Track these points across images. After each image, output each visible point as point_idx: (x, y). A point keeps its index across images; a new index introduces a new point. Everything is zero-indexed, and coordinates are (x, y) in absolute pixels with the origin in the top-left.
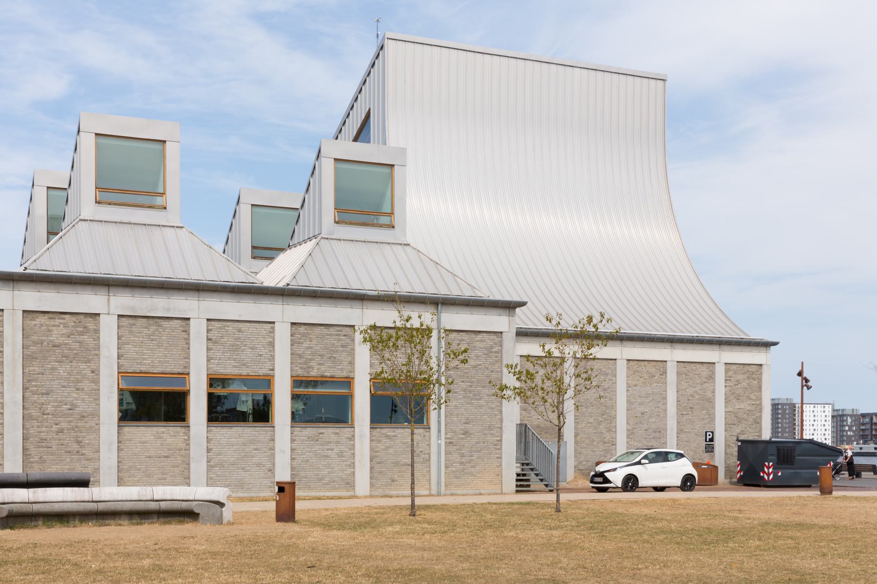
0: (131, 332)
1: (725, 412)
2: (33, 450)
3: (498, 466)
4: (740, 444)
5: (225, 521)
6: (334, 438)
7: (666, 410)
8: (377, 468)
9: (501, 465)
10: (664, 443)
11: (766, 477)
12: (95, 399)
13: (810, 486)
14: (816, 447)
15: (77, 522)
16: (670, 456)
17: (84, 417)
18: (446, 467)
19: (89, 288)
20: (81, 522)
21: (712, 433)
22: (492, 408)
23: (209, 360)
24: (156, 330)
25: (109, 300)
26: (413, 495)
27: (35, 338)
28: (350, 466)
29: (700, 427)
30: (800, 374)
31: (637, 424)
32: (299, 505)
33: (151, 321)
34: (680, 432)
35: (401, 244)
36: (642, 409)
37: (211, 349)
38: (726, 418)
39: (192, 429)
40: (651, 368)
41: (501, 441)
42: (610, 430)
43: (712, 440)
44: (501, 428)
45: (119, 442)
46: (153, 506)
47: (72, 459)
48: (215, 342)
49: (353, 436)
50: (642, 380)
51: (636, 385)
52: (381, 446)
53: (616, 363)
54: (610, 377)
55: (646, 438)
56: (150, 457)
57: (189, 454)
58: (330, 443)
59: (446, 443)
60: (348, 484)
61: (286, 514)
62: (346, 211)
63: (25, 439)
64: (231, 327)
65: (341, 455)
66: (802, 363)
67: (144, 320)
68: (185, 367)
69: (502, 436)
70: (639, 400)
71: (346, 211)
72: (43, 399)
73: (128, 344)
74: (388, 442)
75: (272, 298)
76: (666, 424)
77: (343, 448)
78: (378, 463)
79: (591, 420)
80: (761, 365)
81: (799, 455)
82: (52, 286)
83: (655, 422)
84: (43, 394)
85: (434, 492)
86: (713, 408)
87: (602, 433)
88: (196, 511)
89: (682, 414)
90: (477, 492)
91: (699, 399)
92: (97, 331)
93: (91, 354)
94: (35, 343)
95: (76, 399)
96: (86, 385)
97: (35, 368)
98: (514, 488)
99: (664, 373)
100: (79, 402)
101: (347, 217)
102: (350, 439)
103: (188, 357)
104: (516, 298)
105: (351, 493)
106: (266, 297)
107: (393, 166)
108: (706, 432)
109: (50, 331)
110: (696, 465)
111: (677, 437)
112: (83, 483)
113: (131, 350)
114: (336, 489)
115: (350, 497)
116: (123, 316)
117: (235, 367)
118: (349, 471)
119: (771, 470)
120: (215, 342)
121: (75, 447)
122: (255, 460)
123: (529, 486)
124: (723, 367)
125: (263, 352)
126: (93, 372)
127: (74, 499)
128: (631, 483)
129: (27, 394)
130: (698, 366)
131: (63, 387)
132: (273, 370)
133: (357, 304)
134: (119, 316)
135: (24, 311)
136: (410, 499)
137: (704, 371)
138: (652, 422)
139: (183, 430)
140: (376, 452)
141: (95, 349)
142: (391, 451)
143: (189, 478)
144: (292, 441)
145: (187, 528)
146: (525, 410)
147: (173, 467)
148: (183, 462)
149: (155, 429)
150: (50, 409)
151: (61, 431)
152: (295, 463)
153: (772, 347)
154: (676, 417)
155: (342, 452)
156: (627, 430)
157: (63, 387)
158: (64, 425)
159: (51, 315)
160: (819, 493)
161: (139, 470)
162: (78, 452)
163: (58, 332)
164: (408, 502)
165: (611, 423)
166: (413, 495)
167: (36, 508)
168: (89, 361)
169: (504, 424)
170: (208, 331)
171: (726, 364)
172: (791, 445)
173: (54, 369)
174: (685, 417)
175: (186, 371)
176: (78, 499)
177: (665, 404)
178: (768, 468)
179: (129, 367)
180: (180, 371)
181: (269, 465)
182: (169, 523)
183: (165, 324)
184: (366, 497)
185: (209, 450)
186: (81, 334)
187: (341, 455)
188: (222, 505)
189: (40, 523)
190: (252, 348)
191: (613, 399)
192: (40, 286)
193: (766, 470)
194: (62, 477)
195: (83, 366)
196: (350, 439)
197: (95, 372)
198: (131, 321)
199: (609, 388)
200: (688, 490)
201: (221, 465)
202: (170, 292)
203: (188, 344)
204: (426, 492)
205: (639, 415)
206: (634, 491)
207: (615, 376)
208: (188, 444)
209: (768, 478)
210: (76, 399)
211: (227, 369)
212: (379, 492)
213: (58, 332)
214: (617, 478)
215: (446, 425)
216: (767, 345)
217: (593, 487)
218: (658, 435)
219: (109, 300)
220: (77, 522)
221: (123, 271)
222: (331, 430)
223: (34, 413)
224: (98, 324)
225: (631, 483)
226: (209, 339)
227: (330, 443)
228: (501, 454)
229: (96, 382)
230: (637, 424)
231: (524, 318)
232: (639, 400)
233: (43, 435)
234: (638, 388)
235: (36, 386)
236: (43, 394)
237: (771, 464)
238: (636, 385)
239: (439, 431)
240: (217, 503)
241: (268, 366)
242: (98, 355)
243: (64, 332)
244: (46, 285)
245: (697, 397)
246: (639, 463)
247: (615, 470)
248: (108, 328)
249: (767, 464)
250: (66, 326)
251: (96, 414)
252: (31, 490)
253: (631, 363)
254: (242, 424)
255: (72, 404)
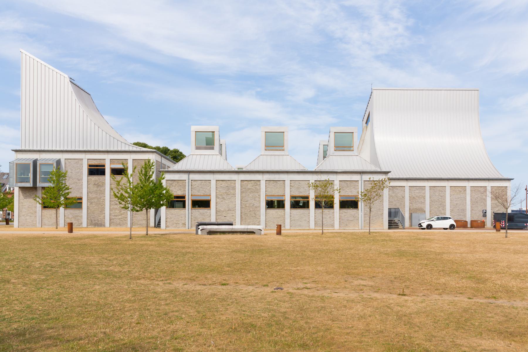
0: (269, 185)
1: (491, 203)
2: (243, 216)
3: (382, 221)
4: (494, 214)
5: (262, 234)
6: (328, 213)
7: (466, 203)
8: (342, 221)
9: (383, 221)
10: (465, 214)
11: (502, 226)
12: (259, 203)
13: (522, 229)
14: (524, 215)
15: (227, 234)
16: (448, 218)
17: (256, 207)
18: (364, 221)
19: (258, 173)
20: (228, 234)
21: (486, 210)
22: (380, 204)
23: (291, 191)
24: (276, 184)
25: (263, 176)
26: (370, 230)
27: (244, 187)
28: (333, 221)
29: (481, 208)
30: (526, 189)
31: (454, 207)
32: (282, 231)
33: (275, 182)
34: (472, 210)
35: (355, 155)
36: (456, 202)
37: (291, 189)
38: (491, 205)
39: (310, 210)
40: (460, 189)
41: (383, 213)
42: (443, 210)
43: (485, 213)
44: (383, 210)
45: (266, 214)
46: (246, 230)
47: (253, 218)
48: (293, 187)
49: (334, 212)
50: (457, 193)
51: (454, 195)
52: (343, 215)
53: (446, 188)
54: (443, 192)
55: (458, 212)
56: (274, 218)
57: (285, 218)
58: (326, 214)
59: (364, 214)
60: (332, 226)
61: (279, 233)
62: (338, 147)
63: (241, 213)
64: (297, 182)
65: (330, 217)
66: (527, 186)
67: (273, 181)
68: (284, 194)
69: (383, 212)
70: (455, 200)
71: (338, 147)
72: (246, 203)
73: (268, 188)
74: (345, 214)
75: (309, 174)
76: (466, 208)
77: (331, 216)
78: (342, 220)
79: (436, 206)
80: (507, 187)
81: (515, 218)
82: (248, 173)
83: (462, 207)
84: (246, 202)
85: (360, 228)
86: (486, 202)
87: (440, 211)
88: (254, 232)
89: (473, 204)
90: (375, 229)
91: (480, 199)
92: (260, 185)
93: (258, 191)
94: (244, 188)
95: (254, 203)
96: (257, 199)
97: (244, 195)
98: (388, 228)
99: (465, 190)
100: (255, 203)
101: (338, 149)
102: (333, 213)
103: (285, 191)
104: (388, 170)
105: (333, 229)
106: (307, 174)
107: (353, 132)
108: (483, 210)
109: (248, 185)
110: (455, 221)
111: (471, 212)
112: (232, 224)
113: (269, 189)
114: (328, 227)
115: (333, 230)
116: (267, 180)
117: (298, 193)
118: (333, 222)
119: (503, 223)
120: (293, 187)
121: (254, 215)
122: (304, 219)
123: (398, 227)
124: (429, 188)
125: (306, 189)
126: (259, 195)
127: (228, 228)
128: (429, 227)
129: (242, 202)
130: (480, 188)
131: (251, 199)
132: (309, 194)
133: (335, 174)
134: (266, 180)
135: (241, 180)
136: (369, 230)
137: (482, 190)
138: (461, 207)
139: (283, 211)
140: (341, 217)
141: (259, 190)
142: (346, 216)
143: (285, 224)
144: (315, 213)
145: (251, 236)
146: (411, 203)
147: (281, 220)
148: (283, 219)
149: (275, 210)
150: (248, 205)
151: (250, 211)
152: (316, 220)
153: (511, 180)
154: (470, 205)
155: (330, 217)
156: (450, 210)
157: (251, 199)
158: (251, 209)
159: (248, 181)
160: (496, 231)
161: (271, 221)
162: (255, 216)
163: (250, 185)
164: (368, 231)
165: (444, 207)
166: (370, 230)
167: (217, 230)
168: (258, 193)
169: (384, 208)
170: (290, 184)
171: (491, 187)
172: (512, 215)
173: (249, 195)
174: (474, 205)
175: (284, 195)
176: (229, 228)
177: (466, 201)
178: (503, 222)
179: (268, 194)
180: (283, 195)
181: (308, 220)
182: (250, 234)
183: (278, 182)
184: (338, 230)
185: (290, 216)
186: (256, 186)
187: (330, 217)
188: (261, 230)
189: (218, 234)
190: (303, 188)
191: (445, 199)
192: (245, 174)
193: (502, 223)
194: (226, 223)
195: (256, 194)
196: (333, 213)
197: (259, 195)
198: (269, 182)
199: (443, 196)
200: (452, 229)
201: (294, 220)
202: (280, 174)
203: (285, 187)
204: (358, 229)
205: (455, 204)
206: (431, 229)
207: (446, 192)
208: (285, 214)
209: (503, 226)
210: (254, 203)
211: (296, 194)
212: (342, 228)
213: (250, 185)
214: (424, 225)
215: (364, 209)
216: (509, 180)
217: (419, 228)
218: (463, 211)
219: (263, 176)
220: (227, 234)
221: (269, 169)
222: (327, 210)
223: (244, 206)
224: (260, 183)
225: (429, 227)
226: (290, 186)
227: (326, 214)
228: (383, 217)
229: (260, 198)
230: (454, 207)
231: (390, 176)
232: (455, 200)
233: (246, 212)
234: (454, 196)
235: (244, 199)
236: (246, 202)
237: (503, 221)
238: (454, 195)
239: (362, 211)
240: (260, 230)
241: (308, 193)
242: (260, 191)
243: (251, 185)
244: (247, 173)
245: (479, 198)
246: (433, 220)
247: (424, 222)
248: (263, 184)
249: (502, 221)
250: (252, 184)
251: (259, 207)
252: (218, 226)
253: (452, 187)
254: (172, 209)
255: (253, 204)
